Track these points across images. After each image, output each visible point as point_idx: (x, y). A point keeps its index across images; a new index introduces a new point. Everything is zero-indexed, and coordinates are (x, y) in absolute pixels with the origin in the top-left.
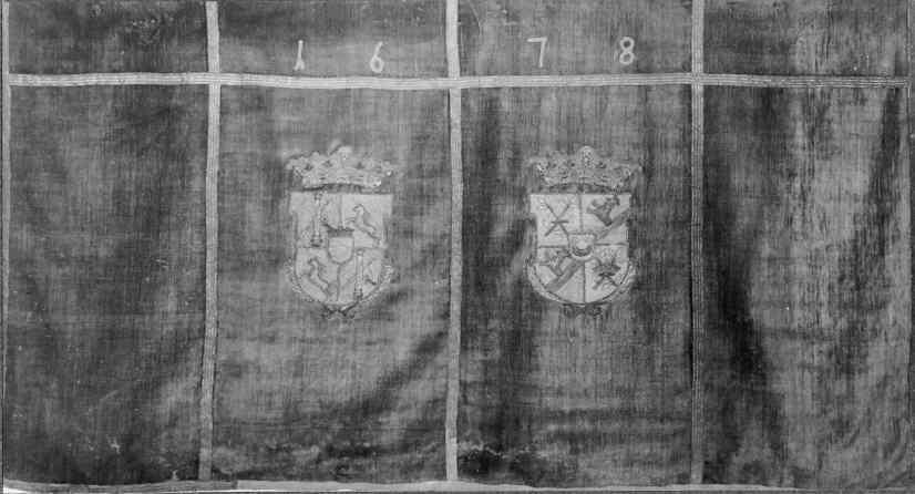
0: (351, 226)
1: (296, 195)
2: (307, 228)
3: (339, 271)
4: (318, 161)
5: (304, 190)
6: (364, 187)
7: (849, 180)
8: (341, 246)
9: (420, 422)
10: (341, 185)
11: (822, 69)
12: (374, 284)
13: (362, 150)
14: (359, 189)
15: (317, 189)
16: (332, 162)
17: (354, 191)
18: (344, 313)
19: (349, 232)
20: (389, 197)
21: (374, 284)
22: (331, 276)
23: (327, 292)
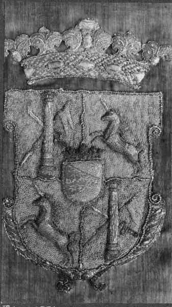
0: (99, 144)
1: (14, 96)
2: (33, 148)
3: (82, 215)
4: (49, 44)
5: (25, 87)
6: (117, 82)
7: (22, 243)
8: (92, 174)
9: (45, 215)
10: (82, 80)
11: (11, 258)
12: (135, 234)
13: (114, 24)
14: (110, 85)
15: (45, 86)
16: (69, 43)
17: (102, 89)
18: (91, 282)
19: (93, 154)
20: (157, 98)
21: (135, 234)
22: (69, 222)
23: (66, 251)
